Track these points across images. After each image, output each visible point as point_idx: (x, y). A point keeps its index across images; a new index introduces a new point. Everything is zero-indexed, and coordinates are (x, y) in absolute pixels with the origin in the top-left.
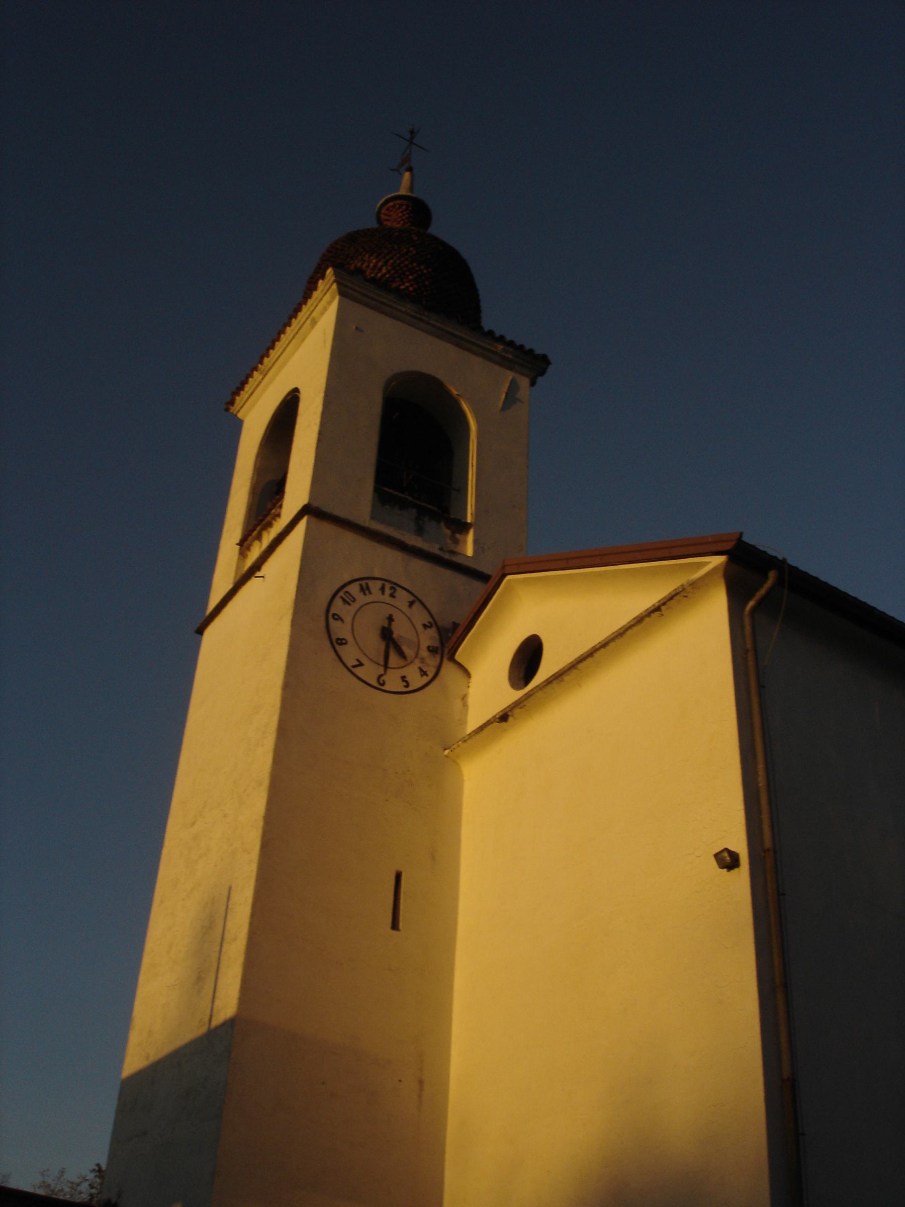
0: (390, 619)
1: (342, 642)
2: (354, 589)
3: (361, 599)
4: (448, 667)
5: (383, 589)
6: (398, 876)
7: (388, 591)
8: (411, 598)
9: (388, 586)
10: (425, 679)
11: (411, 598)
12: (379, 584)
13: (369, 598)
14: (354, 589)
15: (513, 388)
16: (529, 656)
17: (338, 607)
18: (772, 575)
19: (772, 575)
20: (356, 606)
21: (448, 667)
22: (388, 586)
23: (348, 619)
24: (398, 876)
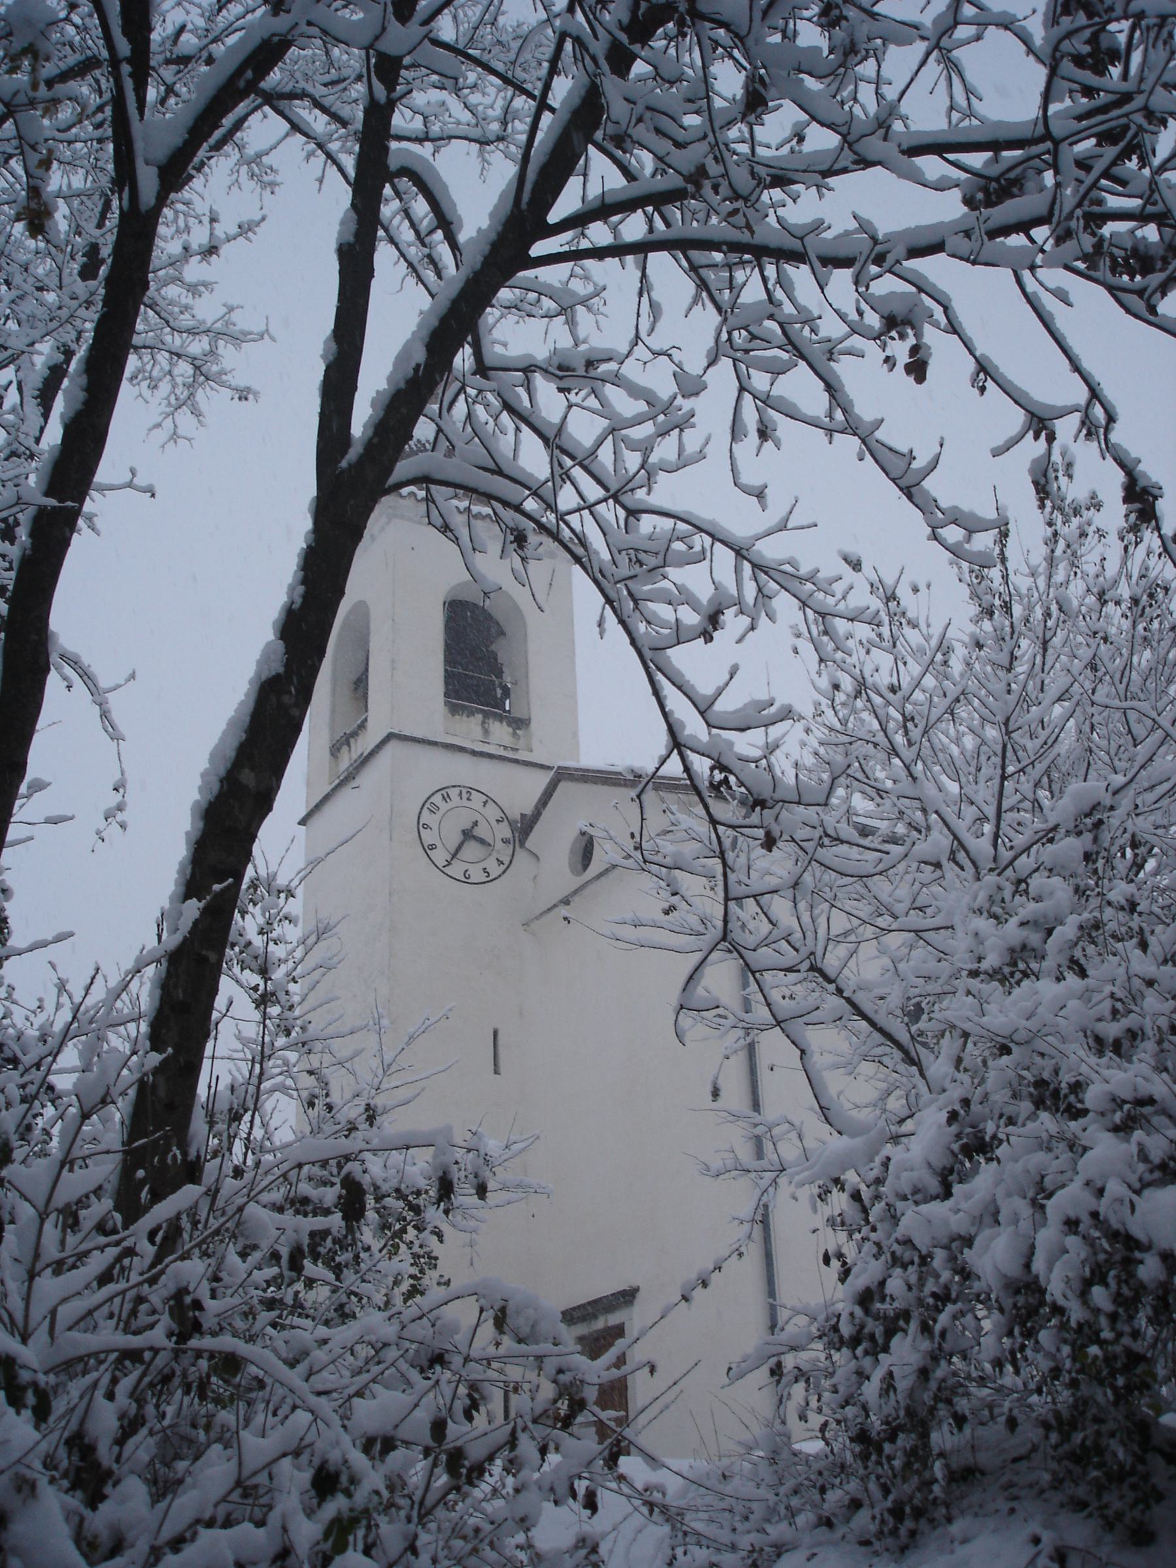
0: (476, 823)
1: (432, 847)
2: (437, 799)
3: (444, 806)
4: (521, 855)
5: (461, 794)
6: (495, 1034)
7: (465, 796)
8: (484, 798)
9: (464, 791)
10: (503, 867)
11: (484, 798)
12: (457, 790)
13: (450, 805)
14: (437, 799)
15: (407, 68)
16: (586, 851)
17: (426, 817)
18: (623, 1413)
19: (623, 1413)
20: (440, 814)
21: (521, 855)
22: (464, 791)
23: (435, 827)
24: (495, 1034)
